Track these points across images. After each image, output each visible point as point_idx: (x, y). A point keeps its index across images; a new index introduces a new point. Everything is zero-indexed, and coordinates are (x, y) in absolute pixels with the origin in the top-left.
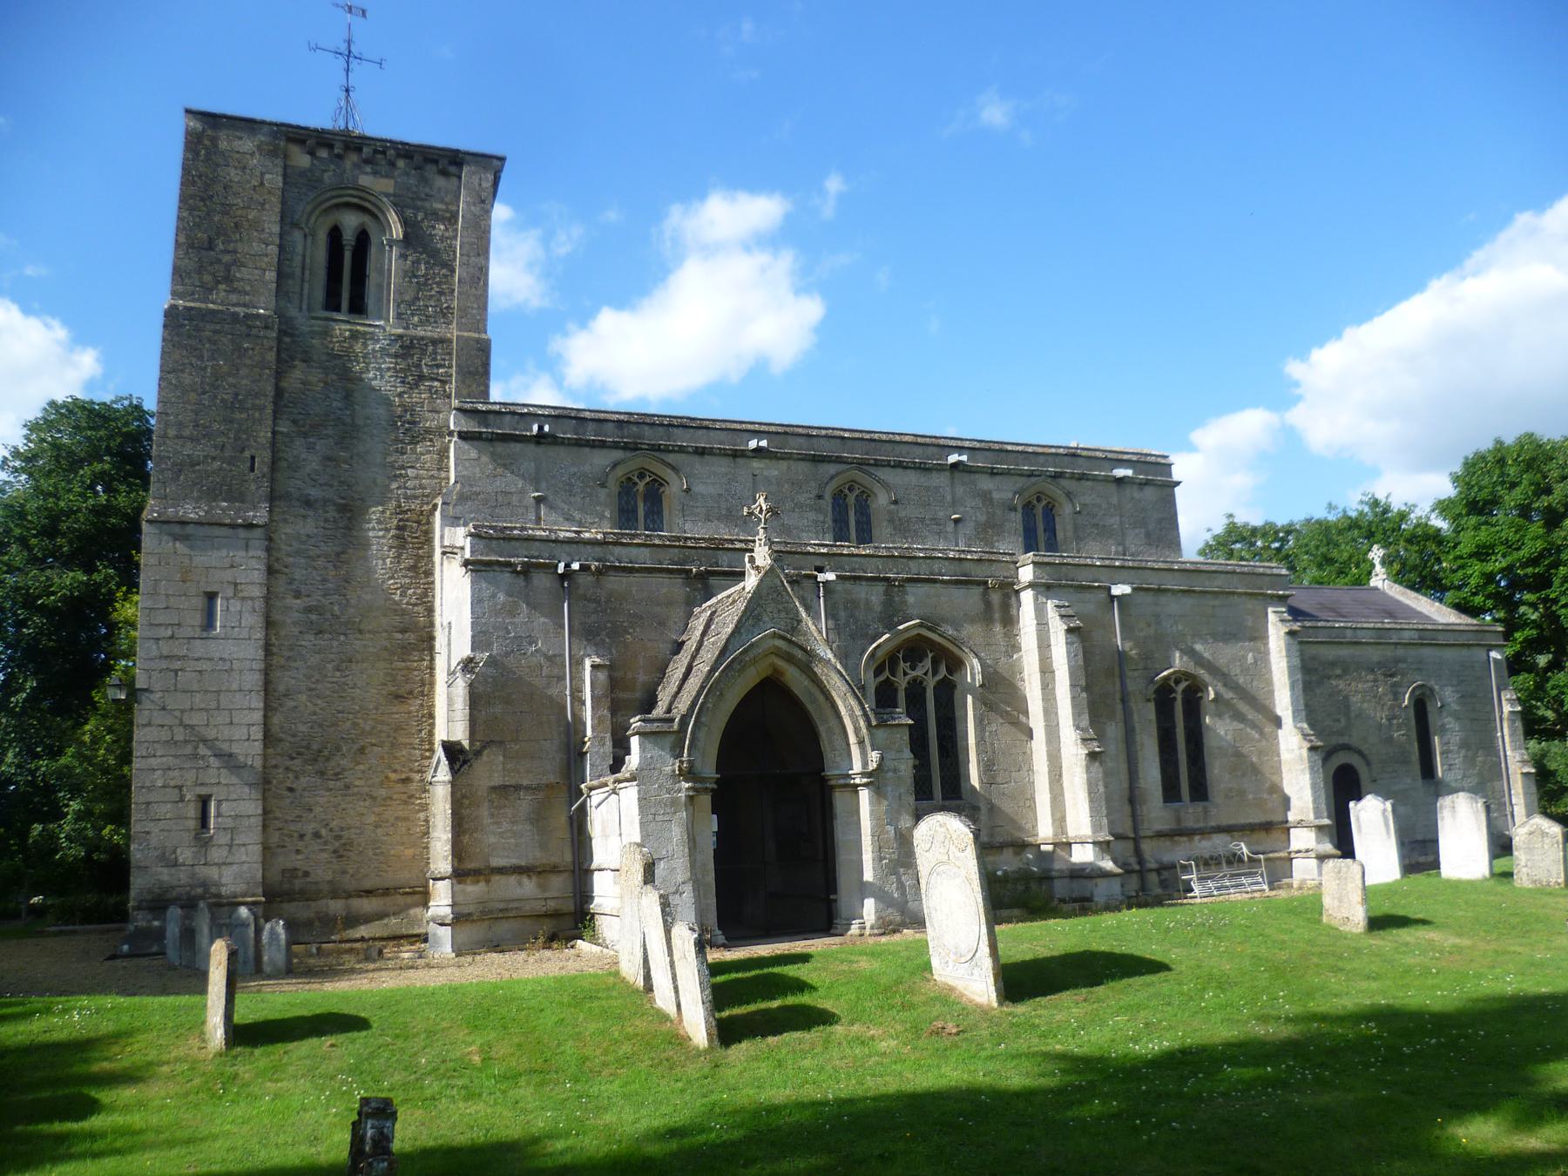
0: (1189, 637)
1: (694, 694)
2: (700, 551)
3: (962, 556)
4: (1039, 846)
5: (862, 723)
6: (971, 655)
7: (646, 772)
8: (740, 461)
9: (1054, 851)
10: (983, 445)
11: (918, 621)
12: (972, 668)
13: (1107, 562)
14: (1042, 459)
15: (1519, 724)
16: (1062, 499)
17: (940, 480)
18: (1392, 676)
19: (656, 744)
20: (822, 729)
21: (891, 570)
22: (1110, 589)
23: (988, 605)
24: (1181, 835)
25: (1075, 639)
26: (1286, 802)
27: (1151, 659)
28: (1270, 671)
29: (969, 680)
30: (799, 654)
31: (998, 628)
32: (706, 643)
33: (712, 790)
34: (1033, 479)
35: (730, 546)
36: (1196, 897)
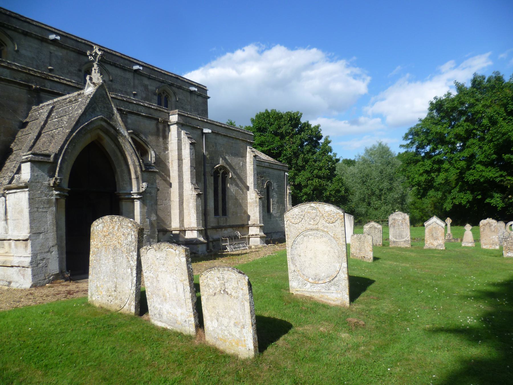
0: (225, 153)
1: (62, 143)
2: (36, 78)
3: (150, 106)
4: (172, 231)
5: (138, 169)
6: (151, 150)
7: (34, 184)
8: (45, 44)
9: (179, 234)
10: (146, 65)
11: (132, 131)
12: (151, 155)
13: (202, 119)
14: (166, 77)
15: (291, 197)
16: (172, 95)
17: (129, 75)
18: (262, 177)
19: (40, 168)
20: (118, 170)
21: (122, 107)
22: (202, 130)
23: (158, 129)
24: (219, 228)
25: (193, 148)
26: (249, 217)
27: (214, 160)
28: (246, 169)
29: (150, 160)
30: (112, 131)
31: (161, 139)
32: (49, 122)
33: (66, 196)
34: (163, 84)
35: (52, 79)
36: (228, 252)
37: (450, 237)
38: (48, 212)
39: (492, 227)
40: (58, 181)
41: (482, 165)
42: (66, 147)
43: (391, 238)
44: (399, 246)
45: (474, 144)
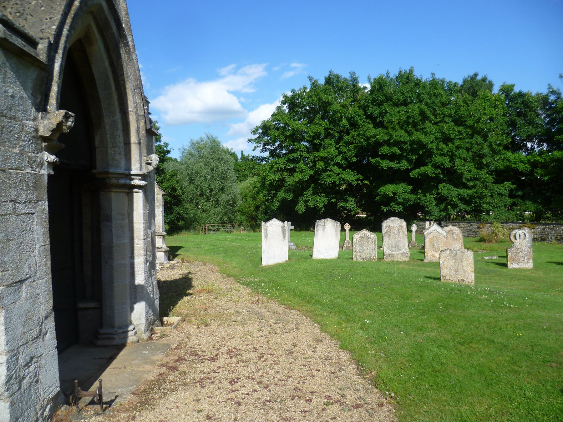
20: (107, 120)
37: (349, 245)
38: (35, 216)
39: (455, 235)
40: (69, 123)
41: (339, 168)
42: (65, 32)
43: (386, 250)
44: (396, 260)
45: (330, 144)
